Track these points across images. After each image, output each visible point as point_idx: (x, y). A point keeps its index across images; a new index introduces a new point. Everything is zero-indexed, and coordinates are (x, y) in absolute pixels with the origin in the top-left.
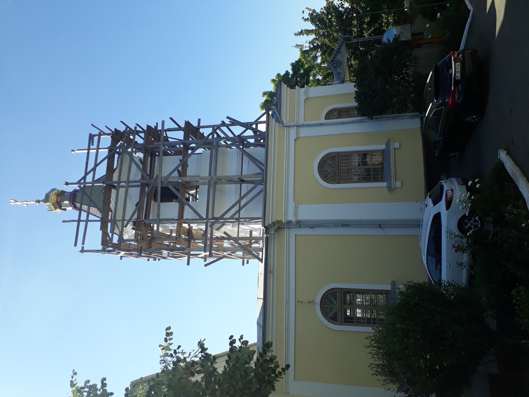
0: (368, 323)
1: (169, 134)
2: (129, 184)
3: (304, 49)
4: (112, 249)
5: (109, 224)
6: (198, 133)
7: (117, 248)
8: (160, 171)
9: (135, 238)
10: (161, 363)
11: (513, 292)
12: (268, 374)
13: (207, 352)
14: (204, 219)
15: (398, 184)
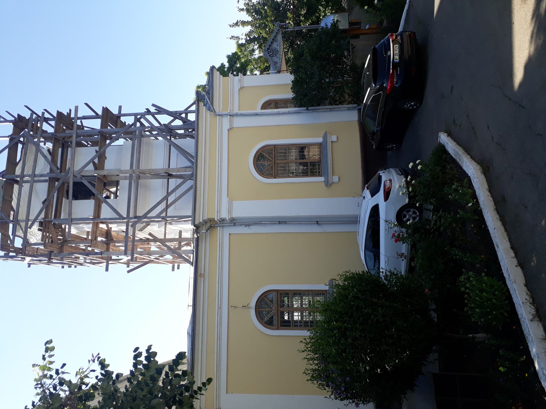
0: (305, 326)
1: (86, 123)
2: (34, 178)
3: (240, 42)
4: (14, 254)
5: (11, 226)
6: (119, 122)
7: (22, 252)
8: (73, 164)
9: (42, 240)
10: (36, 388)
11: (462, 278)
12: (179, 393)
13: (109, 369)
14: (124, 218)
15: (336, 179)
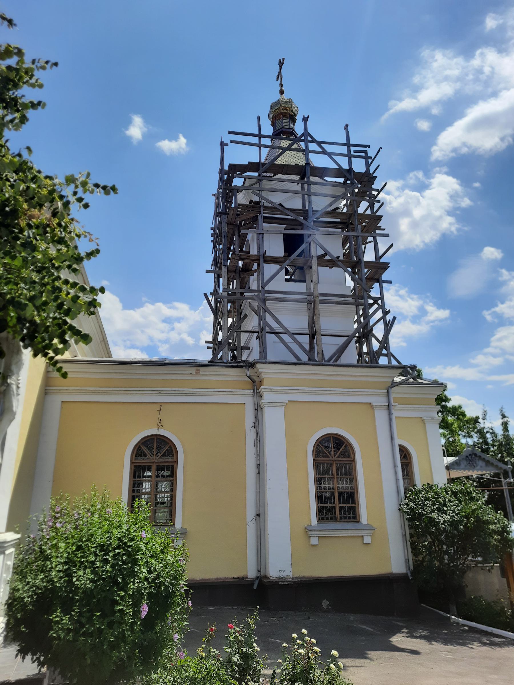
1: (370, 247)
5: (256, 174)
